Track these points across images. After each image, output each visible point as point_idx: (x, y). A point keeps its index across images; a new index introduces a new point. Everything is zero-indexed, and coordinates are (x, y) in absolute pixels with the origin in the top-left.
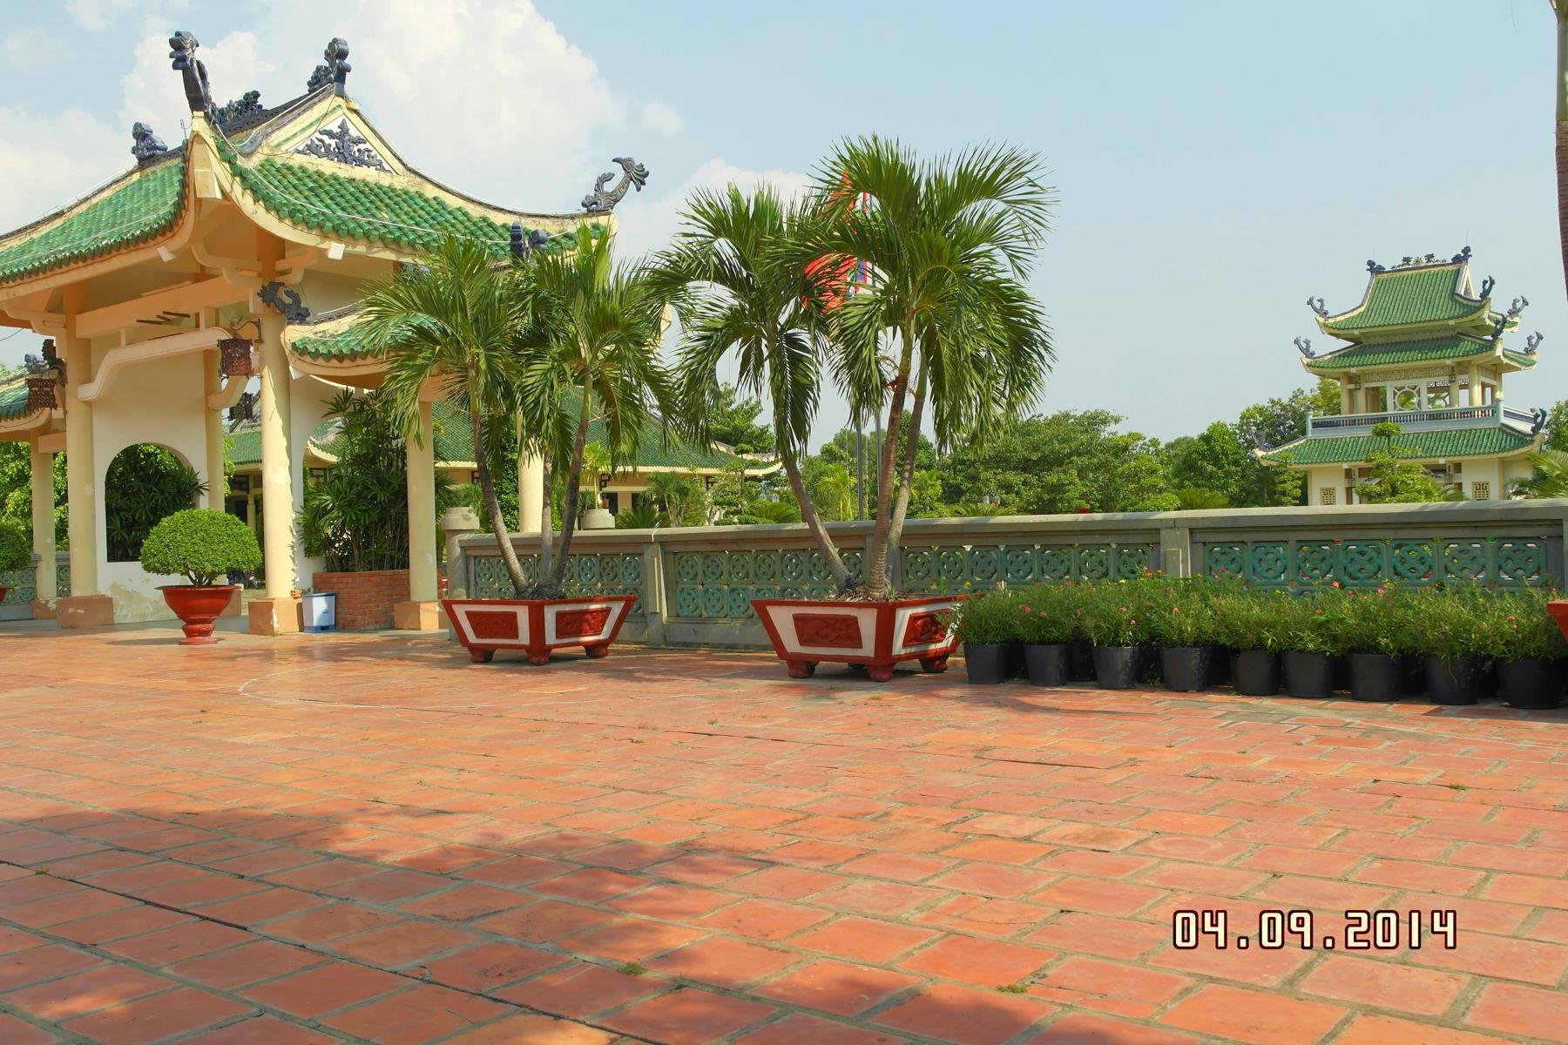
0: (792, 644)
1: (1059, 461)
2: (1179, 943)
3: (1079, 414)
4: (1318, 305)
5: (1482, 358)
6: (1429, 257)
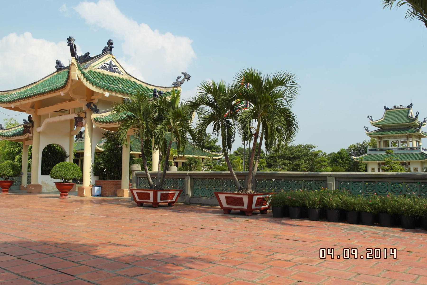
3: (304, 145)
5: (416, 134)
6: (401, 106)
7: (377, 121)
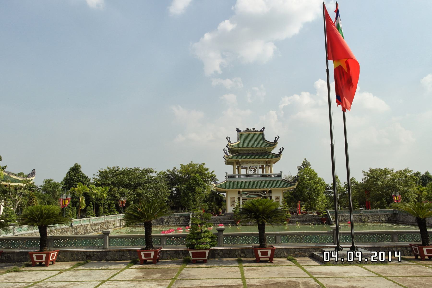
0: (143, 257)
3: (142, 169)
4: (229, 139)
6: (254, 129)
7: (234, 144)
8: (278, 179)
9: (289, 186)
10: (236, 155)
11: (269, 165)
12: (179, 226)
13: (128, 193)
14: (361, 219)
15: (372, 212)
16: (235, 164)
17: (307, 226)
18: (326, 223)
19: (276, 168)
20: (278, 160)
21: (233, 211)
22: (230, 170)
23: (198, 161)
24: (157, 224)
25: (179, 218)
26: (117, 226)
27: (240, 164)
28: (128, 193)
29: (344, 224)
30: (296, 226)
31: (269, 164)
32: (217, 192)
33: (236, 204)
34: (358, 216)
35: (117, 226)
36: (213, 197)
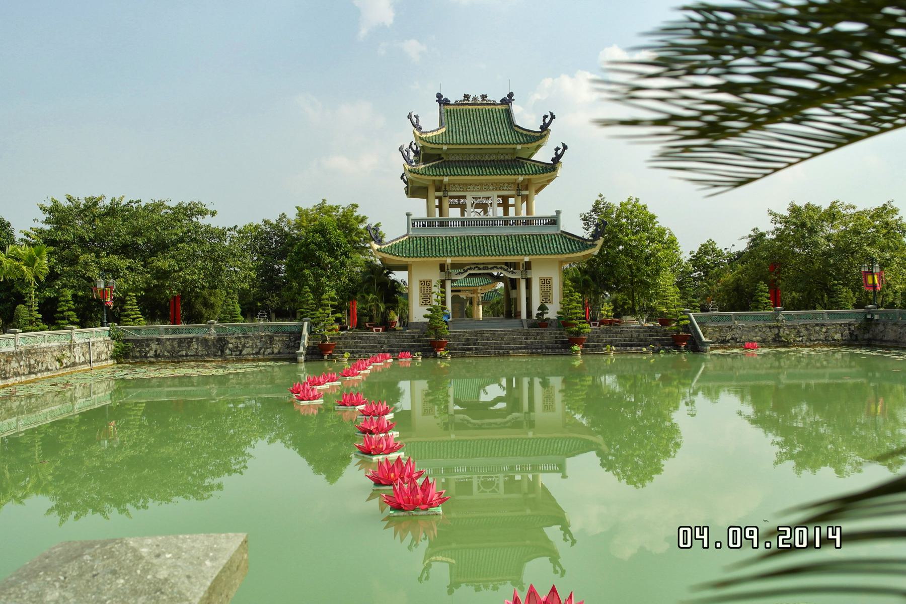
1: (161, 247)
2: (681, 545)
3: (173, 204)
4: (415, 120)
6: (484, 97)
7: (430, 135)
8: (551, 230)
9: (580, 250)
10: (435, 166)
11: (525, 193)
12: (271, 360)
13: (129, 268)
14: (778, 335)
15: (806, 317)
16: (432, 193)
17: (634, 356)
18: (686, 347)
19: (543, 204)
20: (549, 181)
21: (425, 316)
22: (419, 207)
23: (339, 200)
24: (208, 355)
25: (271, 339)
26: (74, 364)
27: (445, 190)
28: (129, 268)
29: (735, 351)
30: (604, 358)
31: (524, 191)
32: (384, 269)
33: (434, 296)
34: (770, 327)
35: (74, 364)
36: (371, 280)
